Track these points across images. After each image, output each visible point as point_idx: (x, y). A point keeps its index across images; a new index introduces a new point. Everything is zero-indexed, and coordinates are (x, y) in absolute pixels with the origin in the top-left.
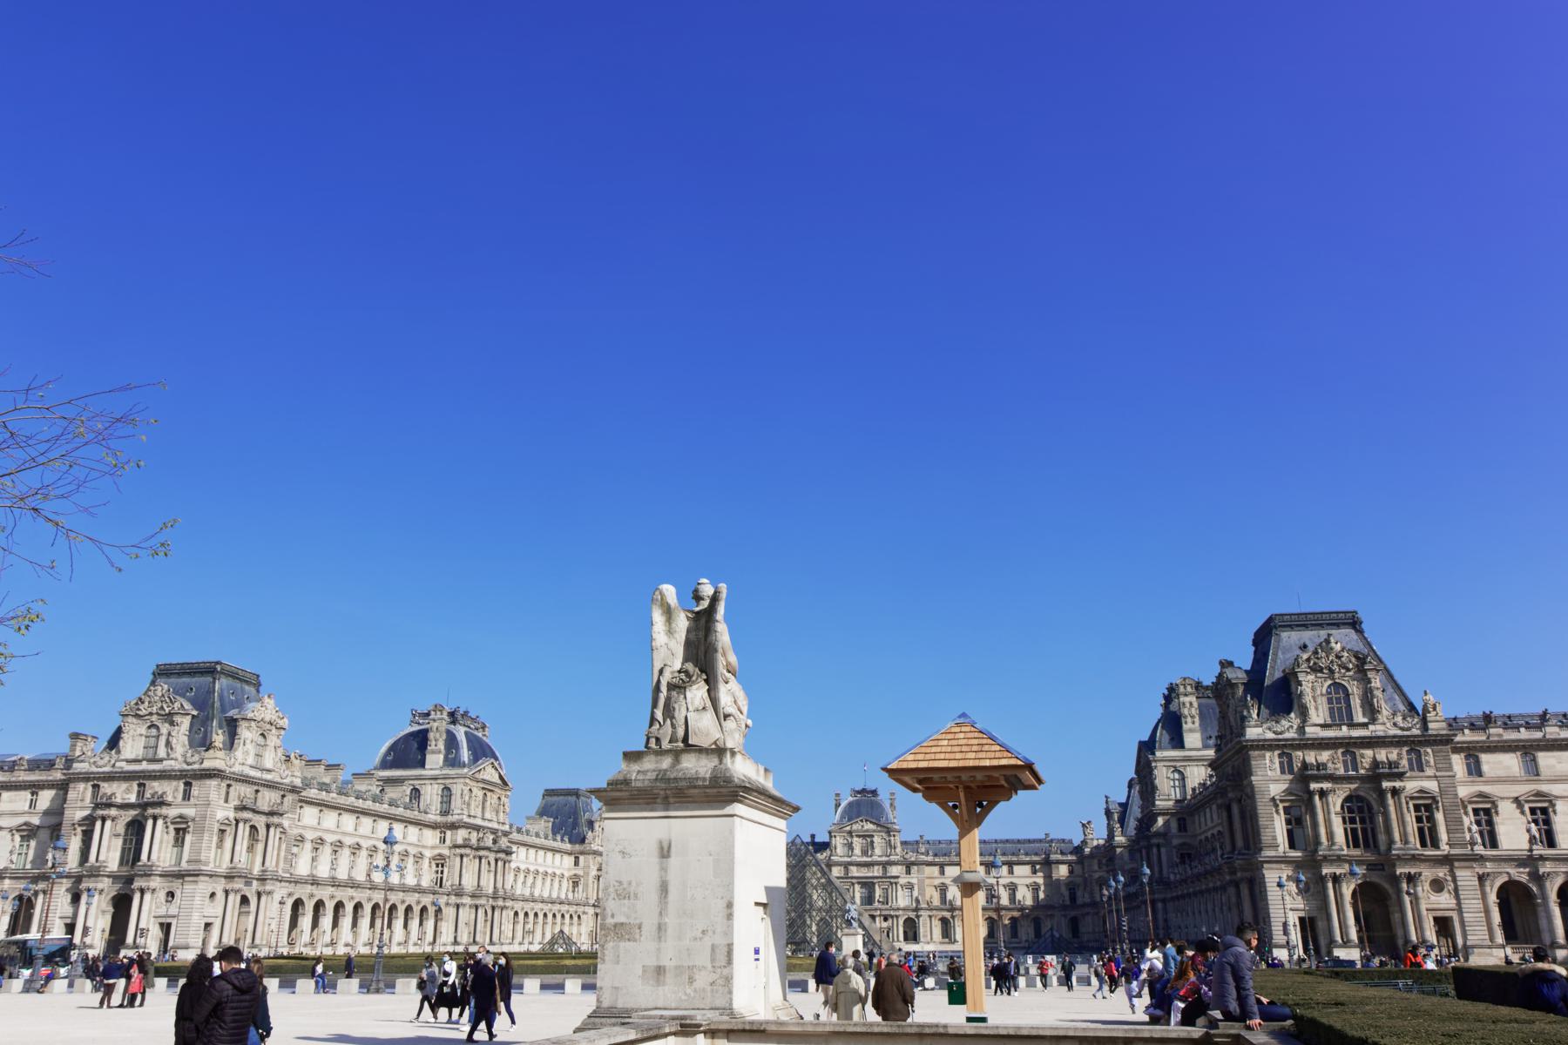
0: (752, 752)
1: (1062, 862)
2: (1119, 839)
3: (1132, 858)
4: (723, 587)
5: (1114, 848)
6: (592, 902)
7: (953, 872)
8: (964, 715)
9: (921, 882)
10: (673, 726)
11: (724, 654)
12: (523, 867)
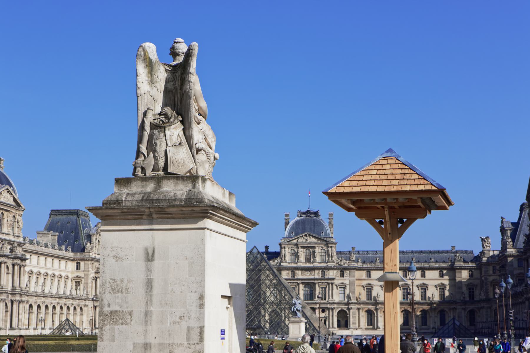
0: (219, 178)
1: (465, 268)
2: (511, 250)
3: (520, 266)
4: (195, 45)
5: (506, 257)
6: (91, 297)
7: (376, 274)
8: (390, 150)
9: (352, 283)
10: (155, 158)
11: (196, 101)
12: (35, 270)
